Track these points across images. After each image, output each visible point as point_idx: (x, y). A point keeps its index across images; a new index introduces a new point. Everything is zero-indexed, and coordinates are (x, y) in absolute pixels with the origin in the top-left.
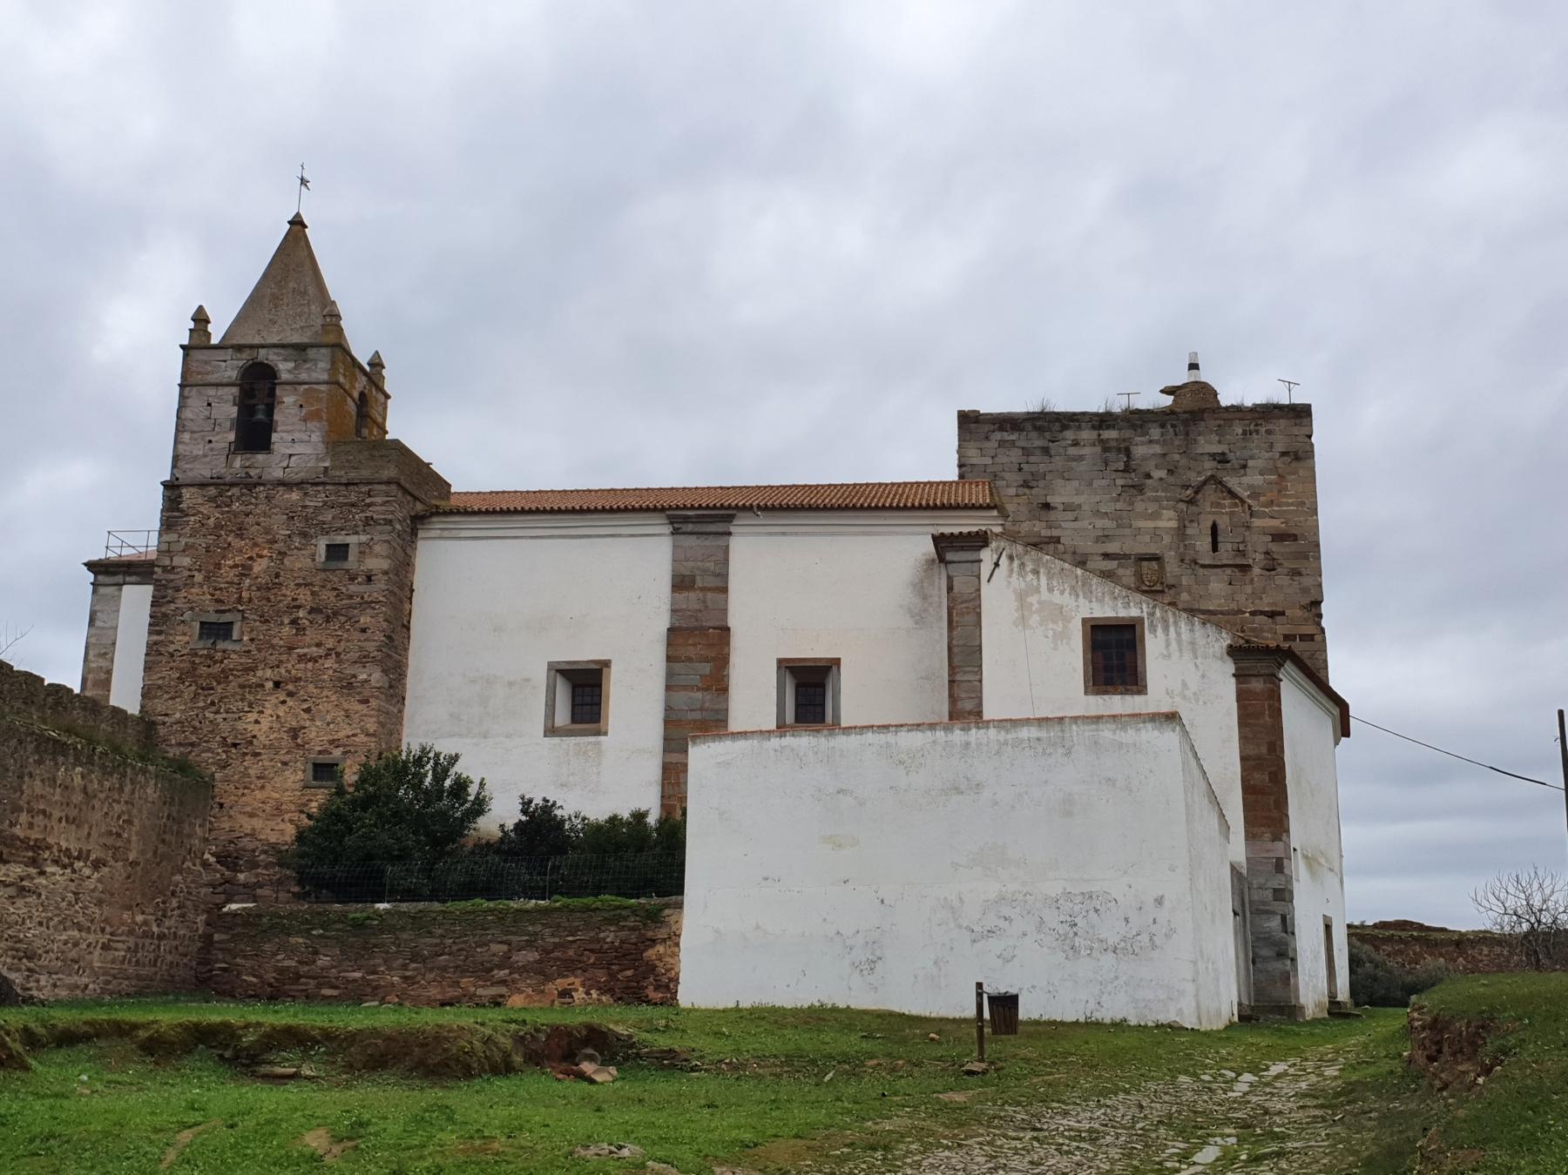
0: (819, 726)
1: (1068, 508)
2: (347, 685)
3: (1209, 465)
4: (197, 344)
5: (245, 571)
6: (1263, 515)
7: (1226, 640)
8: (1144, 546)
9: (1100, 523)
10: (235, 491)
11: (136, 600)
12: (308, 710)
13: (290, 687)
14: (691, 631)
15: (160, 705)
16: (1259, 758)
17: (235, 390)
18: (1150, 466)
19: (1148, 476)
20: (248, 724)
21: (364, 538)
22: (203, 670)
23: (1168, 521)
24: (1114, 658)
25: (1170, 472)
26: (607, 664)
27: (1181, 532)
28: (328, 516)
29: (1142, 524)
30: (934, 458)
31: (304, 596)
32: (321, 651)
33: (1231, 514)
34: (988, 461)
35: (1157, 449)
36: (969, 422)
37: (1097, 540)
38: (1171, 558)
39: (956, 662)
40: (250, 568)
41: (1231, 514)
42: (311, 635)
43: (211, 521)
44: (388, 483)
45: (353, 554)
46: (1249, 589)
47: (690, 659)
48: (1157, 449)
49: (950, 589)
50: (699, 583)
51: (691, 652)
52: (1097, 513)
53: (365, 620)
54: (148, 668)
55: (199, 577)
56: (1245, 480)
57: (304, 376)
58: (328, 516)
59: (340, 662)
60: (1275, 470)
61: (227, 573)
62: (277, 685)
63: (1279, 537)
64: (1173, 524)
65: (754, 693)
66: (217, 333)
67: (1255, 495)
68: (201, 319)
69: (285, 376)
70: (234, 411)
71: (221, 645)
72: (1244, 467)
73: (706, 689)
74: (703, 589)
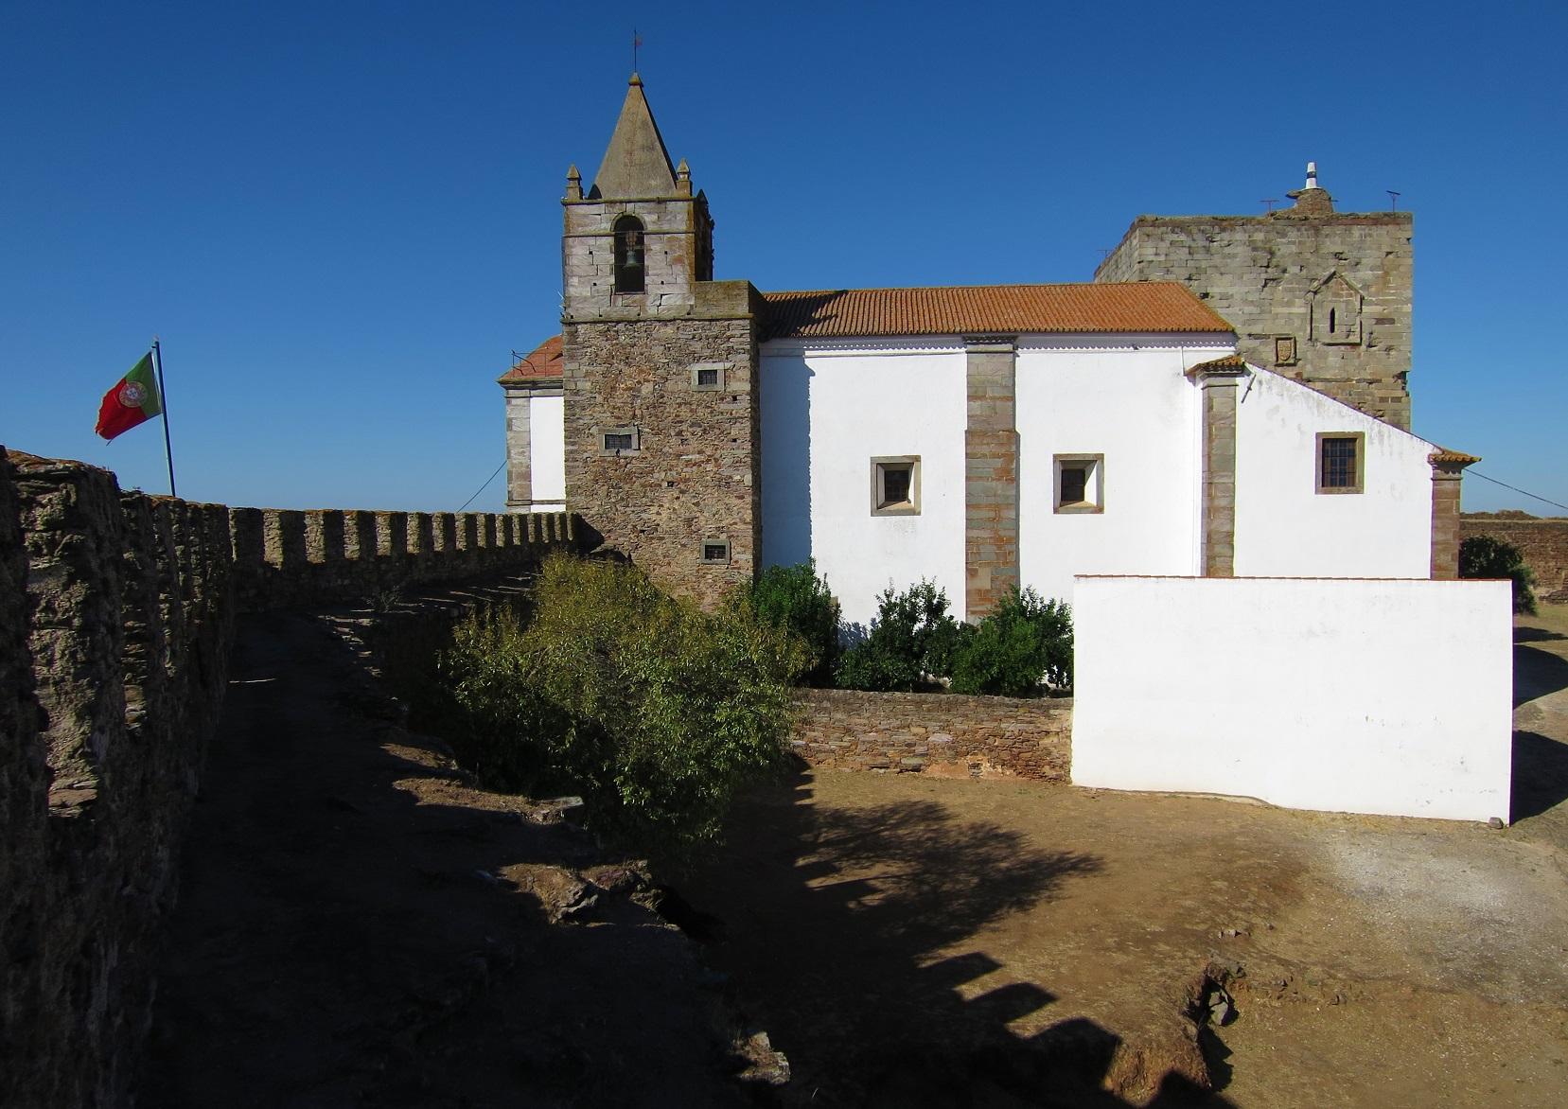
1: (1224, 297)
5: (634, 391)
6: (1371, 303)
7: (1428, 449)
9: (1248, 309)
10: (621, 326)
12: (697, 504)
14: (984, 434)
15: (581, 500)
16: (1446, 542)
17: (611, 240)
18: (1287, 263)
21: (728, 365)
22: (611, 473)
23: (1300, 309)
24: (1338, 464)
28: (697, 346)
29: (1280, 310)
35: (1294, 249)
38: (1302, 337)
39: (1214, 466)
41: (1347, 303)
42: (694, 444)
45: (720, 377)
46: (1356, 362)
48: (1294, 249)
50: (990, 394)
51: (985, 450)
52: (1245, 301)
54: (568, 472)
56: (1360, 274)
57: (666, 227)
58: (697, 346)
59: (719, 466)
60: (1382, 267)
62: (671, 484)
63: (1380, 321)
65: (1037, 483)
69: (650, 228)
70: (612, 258)
71: (623, 453)
74: (993, 398)
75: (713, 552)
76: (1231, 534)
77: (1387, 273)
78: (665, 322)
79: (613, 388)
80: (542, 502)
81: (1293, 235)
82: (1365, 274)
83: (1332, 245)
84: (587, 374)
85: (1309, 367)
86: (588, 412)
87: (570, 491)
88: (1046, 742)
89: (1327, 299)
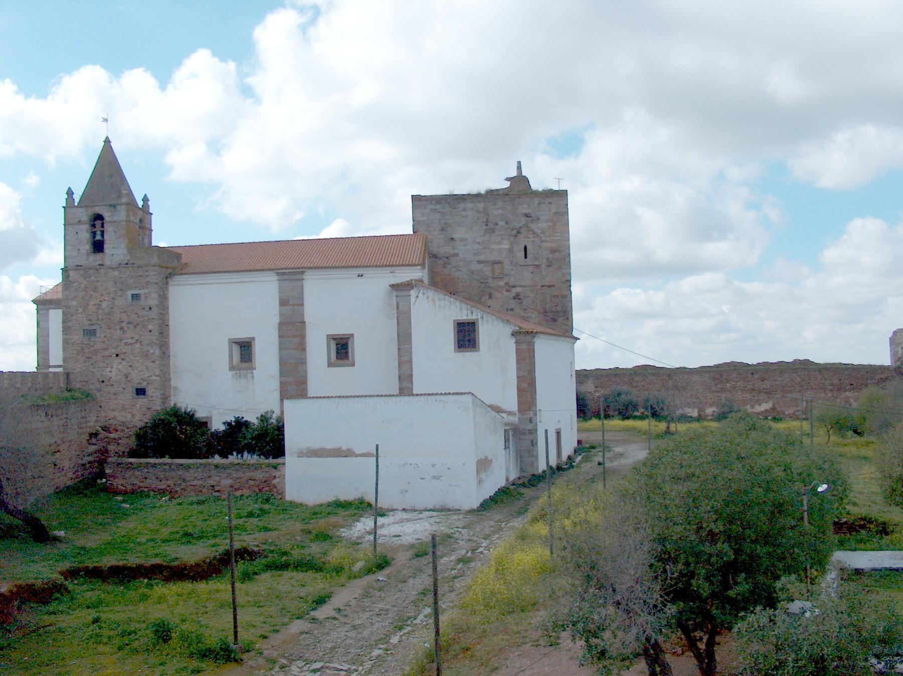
0: (346, 362)
1: (461, 240)
2: (146, 355)
3: (523, 220)
4: (69, 206)
5: (99, 306)
6: (547, 241)
8: (495, 257)
9: (477, 246)
11: (56, 316)
13: (123, 356)
19: (497, 224)
20: (107, 373)
22: (87, 350)
23: (506, 246)
24: (466, 335)
25: (507, 223)
26: (253, 339)
27: (511, 250)
28: (131, 281)
30: (400, 223)
31: (124, 317)
32: (133, 341)
33: (533, 242)
34: (425, 218)
36: (415, 198)
37: (475, 254)
38: (507, 262)
40: (100, 305)
41: (533, 242)
43: (83, 286)
44: (154, 266)
45: (143, 297)
47: (288, 336)
48: (500, 211)
49: (398, 308)
50: (291, 302)
53: (150, 327)
54: (64, 350)
55: (80, 310)
57: (115, 219)
58: (131, 281)
59: (141, 345)
61: (92, 308)
62: (117, 355)
63: (553, 251)
64: (507, 246)
65: (317, 351)
66: (77, 198)
67: (543, 232)
68: (70, 193)
71: (93, 339)
72: (538, 219)
73: (297, 349)
75: (141, 392)
76: (411, 376)
77: (555, 224)
78: (113, 269)
79: (88, 305)
80: (55, 367)
81: (500, 203)
82: (543, 225)
83: (523, 209)
84: (75, 297)
85: (512, 279)
86: (74, 317)
87: (65, 360)
88: (274, 482)
89: (522, 241)
